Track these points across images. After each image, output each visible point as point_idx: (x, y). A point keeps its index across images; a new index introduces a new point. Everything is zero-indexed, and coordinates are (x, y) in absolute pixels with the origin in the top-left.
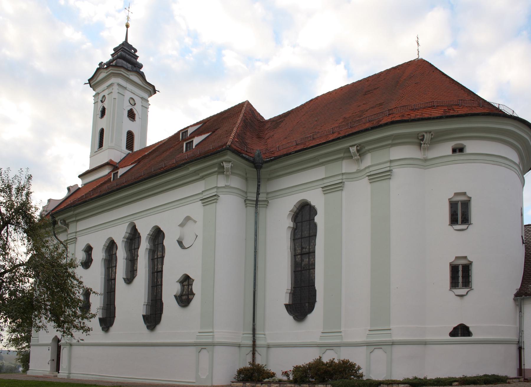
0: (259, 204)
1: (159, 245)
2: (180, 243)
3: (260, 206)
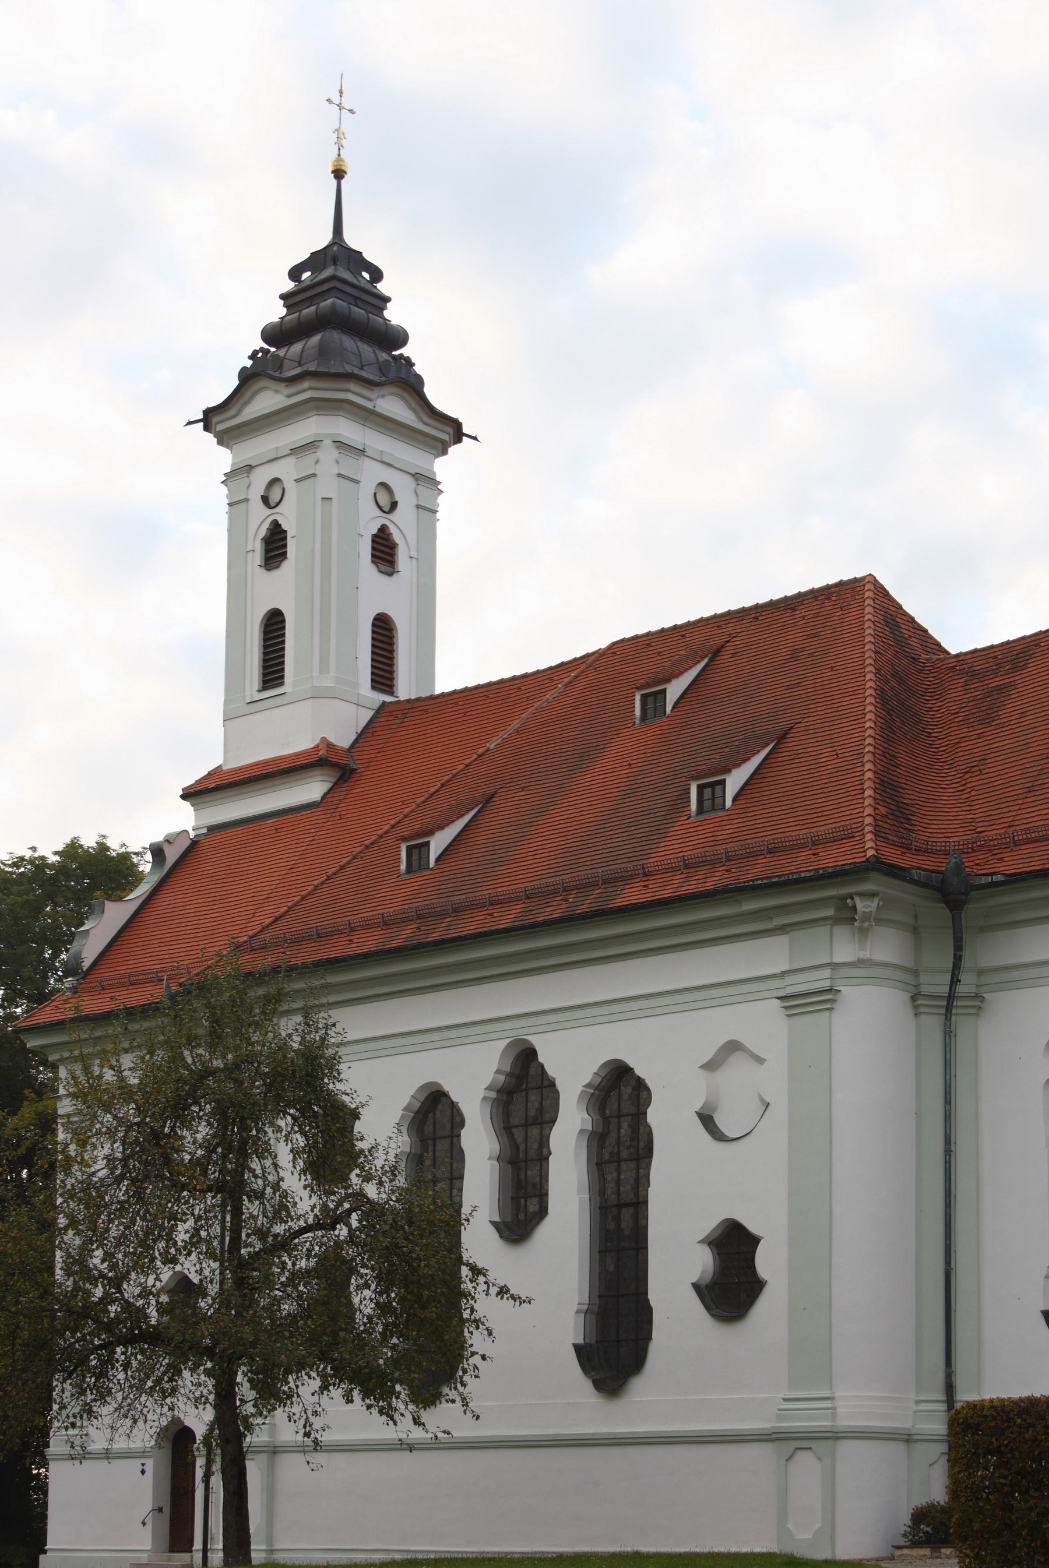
0: (956, 1006)
1: (622, 1119)
2: (707, 1120)
3: (959, 1011)
